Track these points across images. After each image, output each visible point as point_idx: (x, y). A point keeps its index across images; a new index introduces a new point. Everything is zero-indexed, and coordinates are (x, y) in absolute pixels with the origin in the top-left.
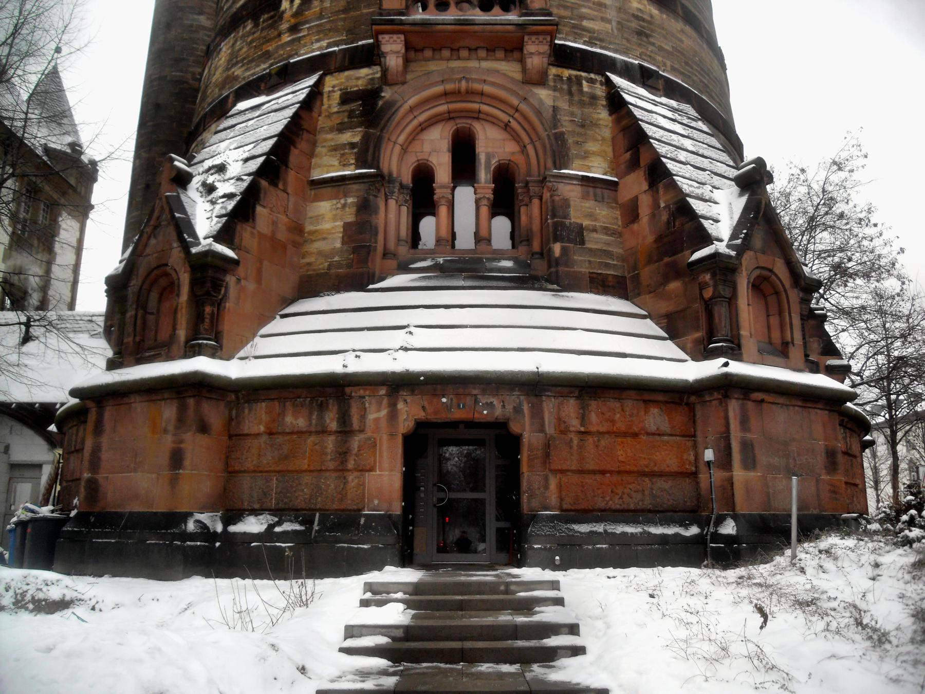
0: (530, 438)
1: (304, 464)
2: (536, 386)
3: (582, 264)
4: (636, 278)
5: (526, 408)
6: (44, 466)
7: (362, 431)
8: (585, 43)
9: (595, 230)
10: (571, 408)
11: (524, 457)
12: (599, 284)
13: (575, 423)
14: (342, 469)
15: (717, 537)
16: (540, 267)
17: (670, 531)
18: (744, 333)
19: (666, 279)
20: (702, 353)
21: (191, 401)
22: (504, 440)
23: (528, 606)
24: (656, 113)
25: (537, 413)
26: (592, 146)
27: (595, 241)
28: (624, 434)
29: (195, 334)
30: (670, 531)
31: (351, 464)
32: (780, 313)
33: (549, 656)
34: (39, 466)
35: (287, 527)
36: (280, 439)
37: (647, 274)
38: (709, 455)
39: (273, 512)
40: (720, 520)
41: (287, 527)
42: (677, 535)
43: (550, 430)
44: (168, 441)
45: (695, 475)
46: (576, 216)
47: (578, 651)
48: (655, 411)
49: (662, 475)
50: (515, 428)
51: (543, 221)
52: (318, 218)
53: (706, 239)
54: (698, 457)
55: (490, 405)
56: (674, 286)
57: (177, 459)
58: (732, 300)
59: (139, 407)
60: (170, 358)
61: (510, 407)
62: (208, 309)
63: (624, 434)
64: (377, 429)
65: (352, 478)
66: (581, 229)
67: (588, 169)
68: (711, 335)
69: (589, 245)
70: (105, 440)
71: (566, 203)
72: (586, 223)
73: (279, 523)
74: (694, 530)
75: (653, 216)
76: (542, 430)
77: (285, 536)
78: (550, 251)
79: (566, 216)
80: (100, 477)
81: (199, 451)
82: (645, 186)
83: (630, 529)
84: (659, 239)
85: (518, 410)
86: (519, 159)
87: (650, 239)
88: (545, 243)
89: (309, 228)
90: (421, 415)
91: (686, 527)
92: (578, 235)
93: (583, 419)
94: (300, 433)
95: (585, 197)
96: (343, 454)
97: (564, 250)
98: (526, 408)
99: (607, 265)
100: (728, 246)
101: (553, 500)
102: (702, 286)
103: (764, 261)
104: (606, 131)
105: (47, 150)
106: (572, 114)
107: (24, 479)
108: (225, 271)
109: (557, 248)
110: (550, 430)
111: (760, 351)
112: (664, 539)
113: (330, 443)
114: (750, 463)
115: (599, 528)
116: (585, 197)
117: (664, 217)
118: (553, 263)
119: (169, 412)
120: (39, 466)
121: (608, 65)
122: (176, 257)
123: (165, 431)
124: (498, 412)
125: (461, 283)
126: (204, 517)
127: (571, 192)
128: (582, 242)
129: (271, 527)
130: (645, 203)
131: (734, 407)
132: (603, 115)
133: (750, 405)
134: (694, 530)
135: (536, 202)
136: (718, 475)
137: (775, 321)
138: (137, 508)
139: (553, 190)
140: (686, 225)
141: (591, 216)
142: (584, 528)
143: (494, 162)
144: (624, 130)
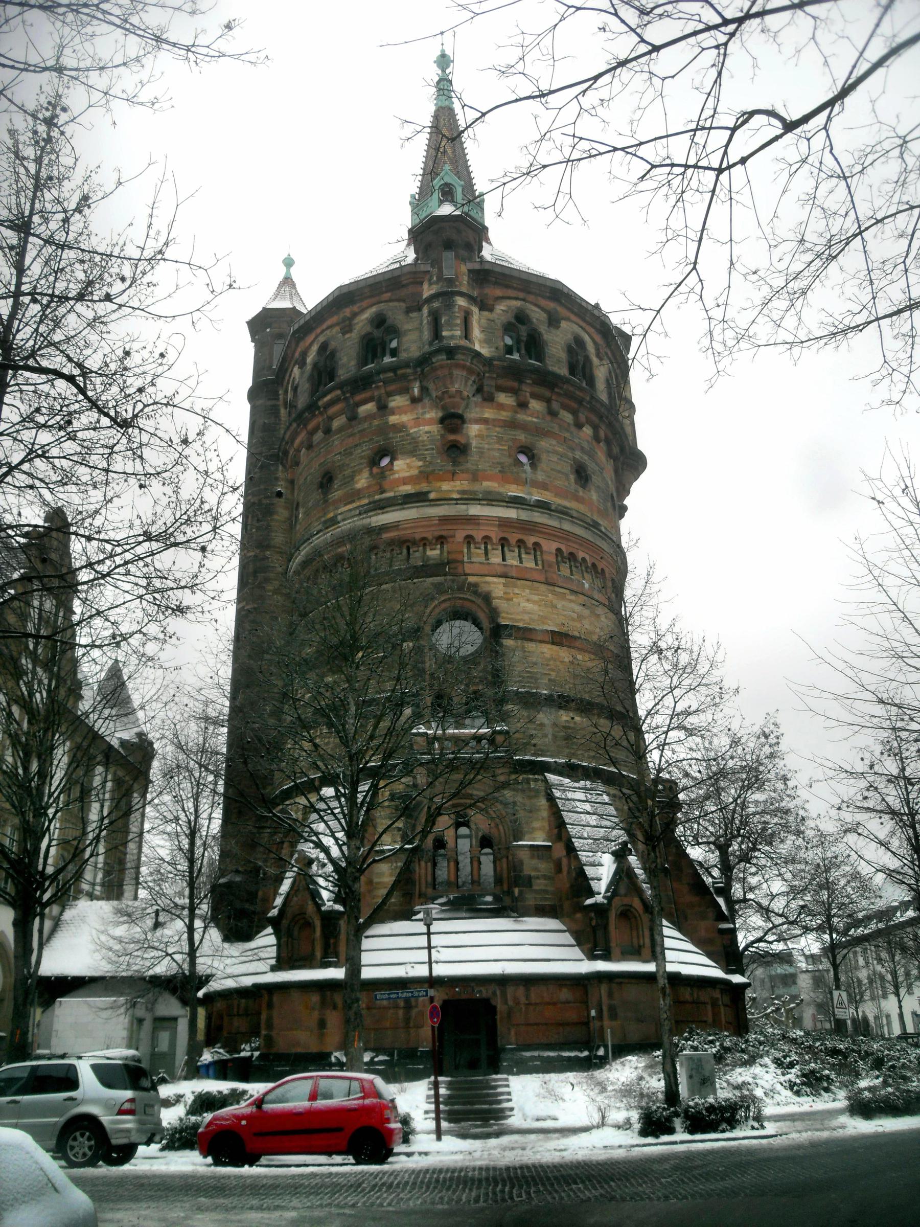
0: (500, 1007)
1: (388, 1025)
2: (503, 981)
3: (531, 899)
4: (561, 906)
5: (498, 993)
6: (180, 1020)
7: (416, 1006)
8: (533, 755)
9: (538, 878)
10: (521, 991)
11: (498, 1017)
12: (541, 912)
13: (523, 1000)
14: (407, 1026)
15: (597, 1057)
16: (507, 901)
17: (572, 1054)
18: (613, 944)
19: (575, 912)
20: (592, 957)
21: (328, 993)
22: (486, 1008)
23: (496, 1087)
24: (574, 800)
25: (504, 995)
26: (536, 824)
27: (539, 884)
28: (549, 1004)
29: (326, 954)
30: (572, 1054)
31: (412, 1024)
32: (637, 929)
33: (500, 1102)
34: (175, 1019)
35: (381, 1058)
36: (374, 1011)
37: (567, 905)
38: (593, 1013)
39: (373, 1050)
40: (598, 1048)
41: (381, 1058)
42: (576, 1057)
43: (510, 1003)
44: (316, 1014)
45: (587, 1024)
46: (527, 871)
47: (510, 1100)
48: (565, 990)
49: (568, 1024)
50: (493, 1002)
51: (509, 873)
52: (381, 874)
53: (591, 893)
54: (589, 1014)
55: (480, 992)
56: (579, 915)
57: (322, 1024)
58: (606, 927)
59: (295, 995)
60: (311, 966)
61: (490, 992)
62: (332, 941)
63: (549, 1004)
64: (424, 1006)
65: (412, 1031)
66: (530, 878)
67: (534, 840)
68: (594, 948)
69: (535, 887)
70: (275, 1013)
71: (521, 863)
72: (533, 874)
73: (377, 1056)
74: (586, 1053)
75: (569, 873)
76: (506, 1002)
77: (381, 1063)
78: (513, 892)
79: (521, 871)
80: (273, 1034)
81: (334, 1019)
82: (564, 853)
83: (552, 1054)
84: (572, 886)
85: (494, 993)
86: (494, 831)
87: (568, 885)
88: (510, 888)
89: (376, 880)
90: (446, 997)
91: (582, 1052)
92: (528, 882)
93: (527, 997)
94: (385, 1008)
95: (532, 857)
96: (407, 1020)
97: (521, 892)
98: (498, 993)
99: (546, 899)
100: (604, 897)
101: (513, 1039)
102: (591, 919)
103: (626, 901)
104: (545, 814)
105: (123, 743)
106: (524, 805)
107: (165, 1029)
108: (339, 919)
109: (516, 891)
110: (510, 1003)
111: (622, 953)
112: (569, 1058)
113: (401, 1013)
114: (613, 1015)
115: (536, 1054)
116: (532, 857)
117: (574, 875)
118: (515, 900)
119: (315, 998)
120: (175, 1019)
121: (545, 768)
122: (310, 908)
123: (313, 1009)
124: (484, 995)
125: (464, 915)
126: (337, 1054)
127: (524, 855)
128: (531, 886)
129: (372, 1059)
130: (565, 862)
131: (604, 988)
132: (543, 802)
133: (614, 985)
134: (586, 1053)
135: (504, 860)
136: (597, 1024)
137: (635, 933)
138: (299, 1050)
139: (513, 855)
140: (581, 884)
141: (536, 869)
142: (528, 1054)
143: (480, 834)
144: (554, 814)
